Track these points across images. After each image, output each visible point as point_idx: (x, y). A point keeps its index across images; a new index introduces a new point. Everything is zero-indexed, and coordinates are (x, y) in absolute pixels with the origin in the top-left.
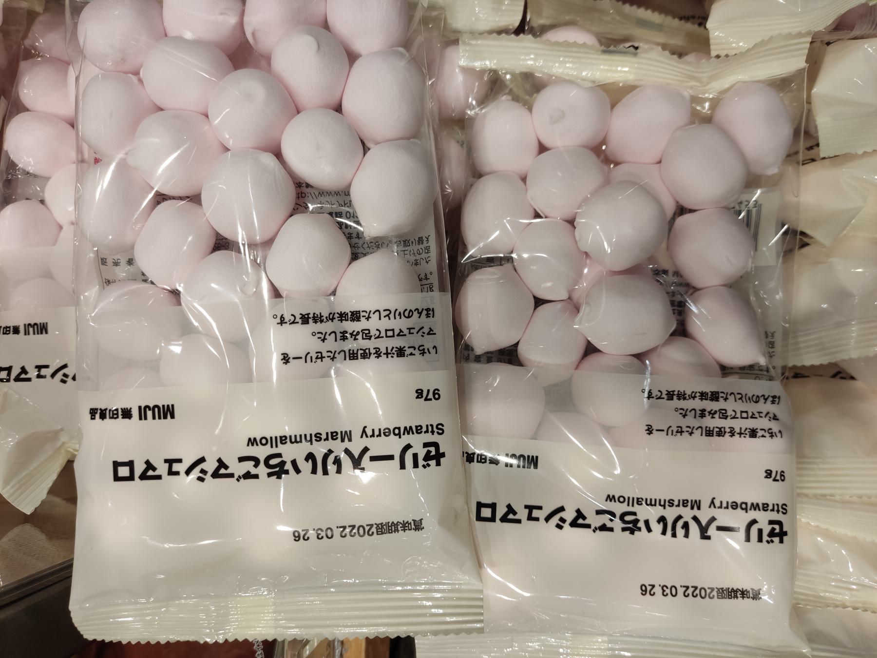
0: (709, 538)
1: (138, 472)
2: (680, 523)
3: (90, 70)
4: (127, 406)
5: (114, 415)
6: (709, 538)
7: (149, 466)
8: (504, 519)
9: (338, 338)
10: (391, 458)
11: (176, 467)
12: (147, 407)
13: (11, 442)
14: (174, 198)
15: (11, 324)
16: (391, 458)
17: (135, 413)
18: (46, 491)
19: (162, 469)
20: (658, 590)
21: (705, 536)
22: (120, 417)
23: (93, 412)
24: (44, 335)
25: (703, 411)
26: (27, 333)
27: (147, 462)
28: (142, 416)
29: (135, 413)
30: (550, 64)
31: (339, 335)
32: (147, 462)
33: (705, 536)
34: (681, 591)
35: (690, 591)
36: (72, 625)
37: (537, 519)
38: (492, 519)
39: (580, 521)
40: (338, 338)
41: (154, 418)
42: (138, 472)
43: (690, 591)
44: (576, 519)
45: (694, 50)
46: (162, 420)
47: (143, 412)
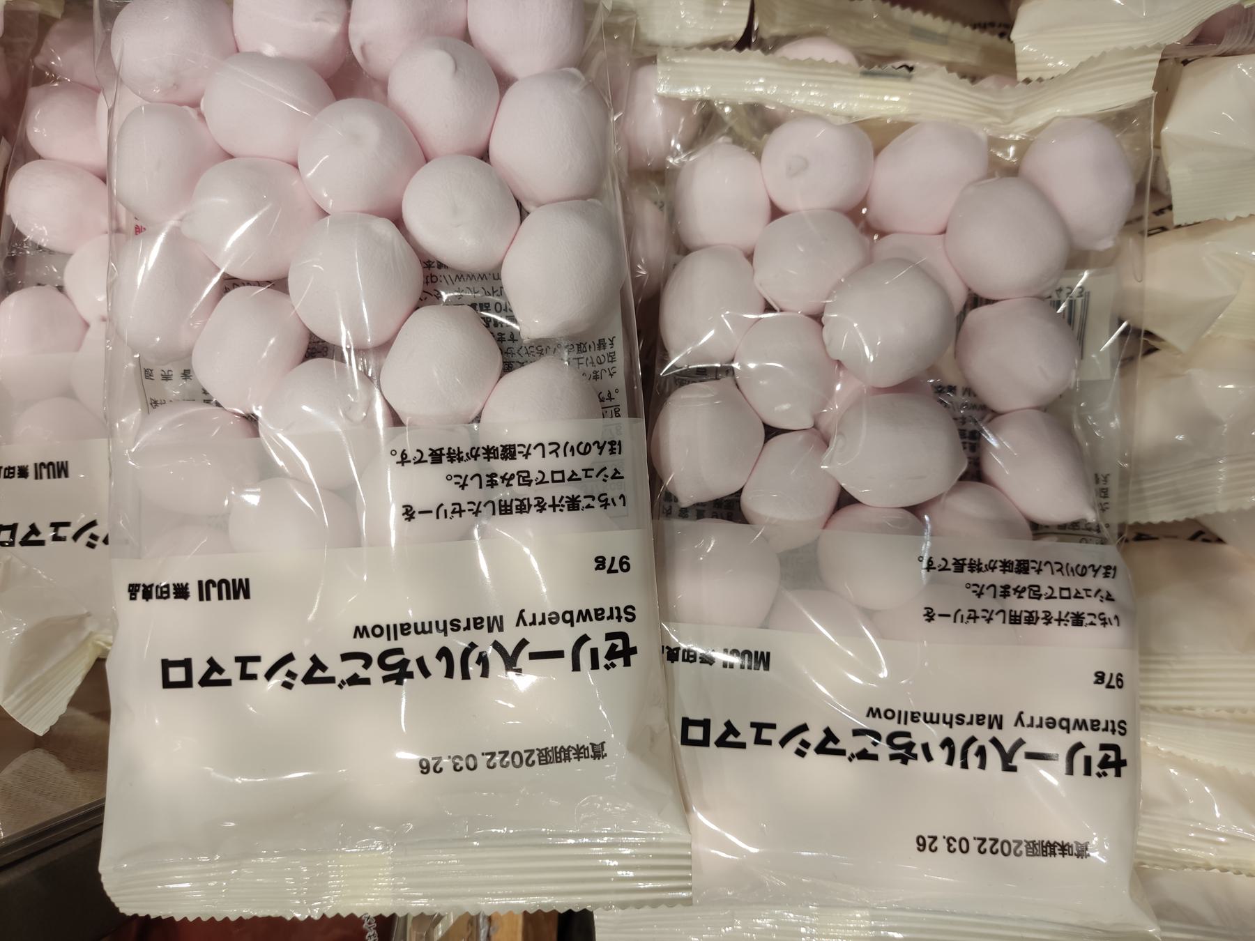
0: (1014, 769)
1: (197, 674)
2: (973, 749)
3: (129, 101)
4: (181, 580)
5: (163, 594)
6: (1014, 769)
7: (214, 666)
8: (721, 742)
9: (484, 483)
10: (559, 654)
11: (252, 668)
12: (210, 582)
14: (249, 283)
15: (16, 463)
16: (559, 654)
17: (193, 590)
18: (65, 703)
19: (232, 670)
20: (941, 844)
21: (1008, 767)
22: (172, 596)
23: (133, 590)
24: (63, 479)
25: (1006, 587)
26: (38, 476)
27: (211, 661)
28: (204, 595)
29: (193, 590)
30: (788, 92)
31: (485, 479)
32: (211, 661)
33: (1008, 767)
34: (974, 845)
35: (988, 845)
36: (103, 893)
37: (769, 743)
38: (705, 742)
39: (831, 745)
40: (484, 483)
41: (220, 598)
42: (197, 674)
43: (988, 845)
44: (824, 742)
45: (993, 72)
46: (232, 601)
47: (205, 590)
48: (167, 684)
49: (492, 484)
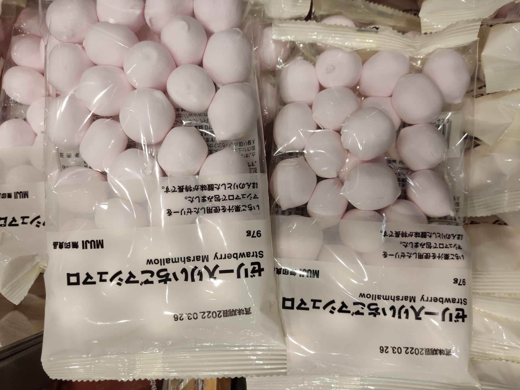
0: (420, 319)
1: (82, 280)
2: (403, 310)
4: (75, 240)
5: (68, 246)
6: (420, 319)
7: (89, 276)
8: (299, 308)
9: (201, 200)
10: (232, 271)
11: (104, 277)
12: (87, 241)
14: (103, 117)
16: (232, 271)
17: (80, 245)
19: (96, 278)
21: (418, 318)
22: (71, 247)
24: (26, 198)
25: (417, 243)
27: (87, 274)
28: (84, 246)
29: (80, 245)
30: (326, 38)
31: (201, 199)
32: (87, 274)
33: (418, 318)
34: (404, 350)
35: (409, 350)
36: (43, 370)
37: (318, 308)
38: (292, 308)
39: (344, 309)
40: (201, 200)
41: (91, 248)
42: (82, 280)
43: (409, 350)
44: (341, 308)
45: (411, 30)
46: (96, 249)
47: (85, 244)
48: (69, 283)
49: (204, 200)
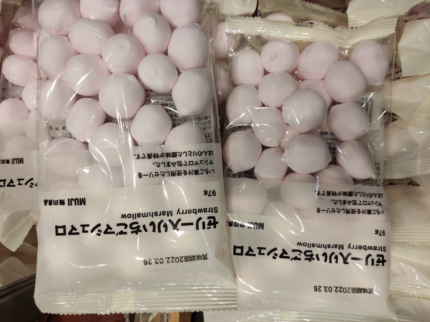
0: (347, 263)
1: (68, 231)
2: (333, 256)
3: (44, 34)
4: (62, 199)
5: (56, 203)
6: (347, 263)
7: (73, 228)
8: (247, 254)
9: (166, 165)
10: (192, 224)
11: (86, 229)
12: (72, 199)
13: (5, 216)
15: (5, 158)
16: (192, 224)
17: (66, 202)
19: (79, 229)
20: (322, 289)
21: (345, 262)
22: (59, 204)
23: (46, 202)
24: (22, 164)
27: (72, 226)
28: (70, 203)
29: (66, 202)
30: (270, 31)
31: (166, 164)
32: (72, 226)
33: (345, 262)
34: (334, 289)
35: (338, 289)
36: (35, 306)
37: (263, 254)
38: (241, 254)
39: (285, 255)
40: (166, 165)
41: (75, 205)
42: (68, 231)
43: (338, 289)
44: (282, 254)
46: (80, 206)
47: (70, 202)
49: (169, 166)
